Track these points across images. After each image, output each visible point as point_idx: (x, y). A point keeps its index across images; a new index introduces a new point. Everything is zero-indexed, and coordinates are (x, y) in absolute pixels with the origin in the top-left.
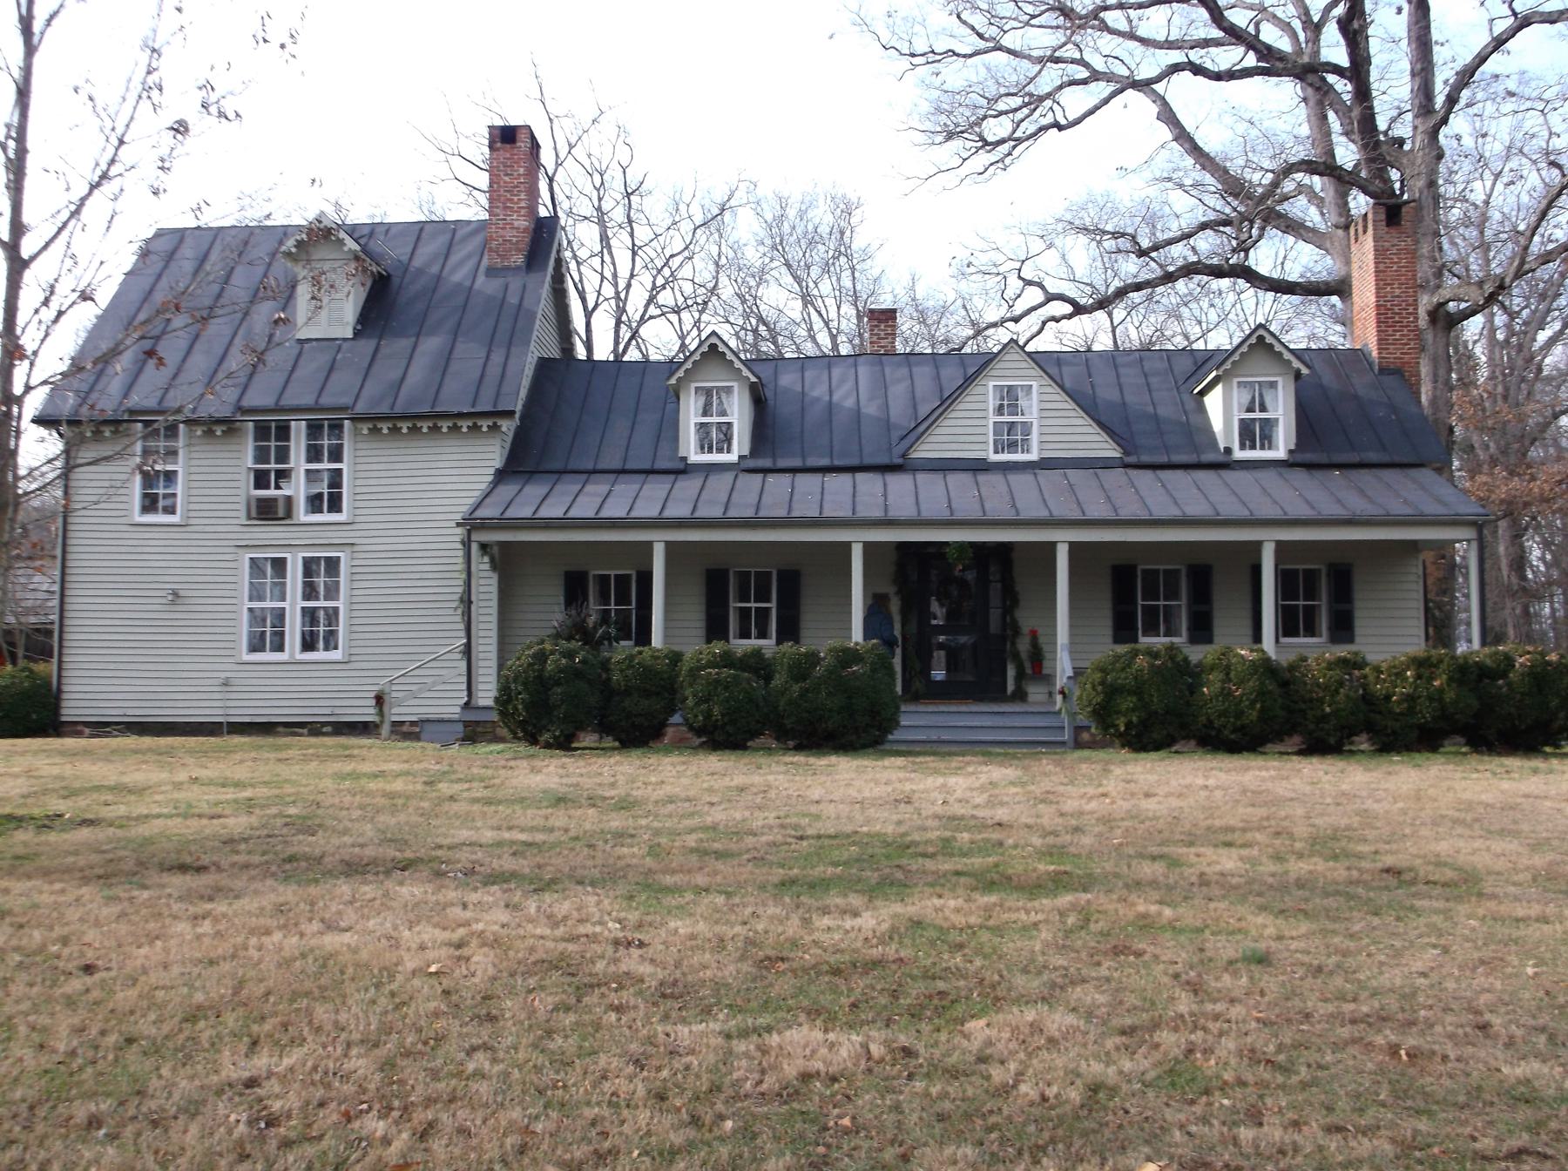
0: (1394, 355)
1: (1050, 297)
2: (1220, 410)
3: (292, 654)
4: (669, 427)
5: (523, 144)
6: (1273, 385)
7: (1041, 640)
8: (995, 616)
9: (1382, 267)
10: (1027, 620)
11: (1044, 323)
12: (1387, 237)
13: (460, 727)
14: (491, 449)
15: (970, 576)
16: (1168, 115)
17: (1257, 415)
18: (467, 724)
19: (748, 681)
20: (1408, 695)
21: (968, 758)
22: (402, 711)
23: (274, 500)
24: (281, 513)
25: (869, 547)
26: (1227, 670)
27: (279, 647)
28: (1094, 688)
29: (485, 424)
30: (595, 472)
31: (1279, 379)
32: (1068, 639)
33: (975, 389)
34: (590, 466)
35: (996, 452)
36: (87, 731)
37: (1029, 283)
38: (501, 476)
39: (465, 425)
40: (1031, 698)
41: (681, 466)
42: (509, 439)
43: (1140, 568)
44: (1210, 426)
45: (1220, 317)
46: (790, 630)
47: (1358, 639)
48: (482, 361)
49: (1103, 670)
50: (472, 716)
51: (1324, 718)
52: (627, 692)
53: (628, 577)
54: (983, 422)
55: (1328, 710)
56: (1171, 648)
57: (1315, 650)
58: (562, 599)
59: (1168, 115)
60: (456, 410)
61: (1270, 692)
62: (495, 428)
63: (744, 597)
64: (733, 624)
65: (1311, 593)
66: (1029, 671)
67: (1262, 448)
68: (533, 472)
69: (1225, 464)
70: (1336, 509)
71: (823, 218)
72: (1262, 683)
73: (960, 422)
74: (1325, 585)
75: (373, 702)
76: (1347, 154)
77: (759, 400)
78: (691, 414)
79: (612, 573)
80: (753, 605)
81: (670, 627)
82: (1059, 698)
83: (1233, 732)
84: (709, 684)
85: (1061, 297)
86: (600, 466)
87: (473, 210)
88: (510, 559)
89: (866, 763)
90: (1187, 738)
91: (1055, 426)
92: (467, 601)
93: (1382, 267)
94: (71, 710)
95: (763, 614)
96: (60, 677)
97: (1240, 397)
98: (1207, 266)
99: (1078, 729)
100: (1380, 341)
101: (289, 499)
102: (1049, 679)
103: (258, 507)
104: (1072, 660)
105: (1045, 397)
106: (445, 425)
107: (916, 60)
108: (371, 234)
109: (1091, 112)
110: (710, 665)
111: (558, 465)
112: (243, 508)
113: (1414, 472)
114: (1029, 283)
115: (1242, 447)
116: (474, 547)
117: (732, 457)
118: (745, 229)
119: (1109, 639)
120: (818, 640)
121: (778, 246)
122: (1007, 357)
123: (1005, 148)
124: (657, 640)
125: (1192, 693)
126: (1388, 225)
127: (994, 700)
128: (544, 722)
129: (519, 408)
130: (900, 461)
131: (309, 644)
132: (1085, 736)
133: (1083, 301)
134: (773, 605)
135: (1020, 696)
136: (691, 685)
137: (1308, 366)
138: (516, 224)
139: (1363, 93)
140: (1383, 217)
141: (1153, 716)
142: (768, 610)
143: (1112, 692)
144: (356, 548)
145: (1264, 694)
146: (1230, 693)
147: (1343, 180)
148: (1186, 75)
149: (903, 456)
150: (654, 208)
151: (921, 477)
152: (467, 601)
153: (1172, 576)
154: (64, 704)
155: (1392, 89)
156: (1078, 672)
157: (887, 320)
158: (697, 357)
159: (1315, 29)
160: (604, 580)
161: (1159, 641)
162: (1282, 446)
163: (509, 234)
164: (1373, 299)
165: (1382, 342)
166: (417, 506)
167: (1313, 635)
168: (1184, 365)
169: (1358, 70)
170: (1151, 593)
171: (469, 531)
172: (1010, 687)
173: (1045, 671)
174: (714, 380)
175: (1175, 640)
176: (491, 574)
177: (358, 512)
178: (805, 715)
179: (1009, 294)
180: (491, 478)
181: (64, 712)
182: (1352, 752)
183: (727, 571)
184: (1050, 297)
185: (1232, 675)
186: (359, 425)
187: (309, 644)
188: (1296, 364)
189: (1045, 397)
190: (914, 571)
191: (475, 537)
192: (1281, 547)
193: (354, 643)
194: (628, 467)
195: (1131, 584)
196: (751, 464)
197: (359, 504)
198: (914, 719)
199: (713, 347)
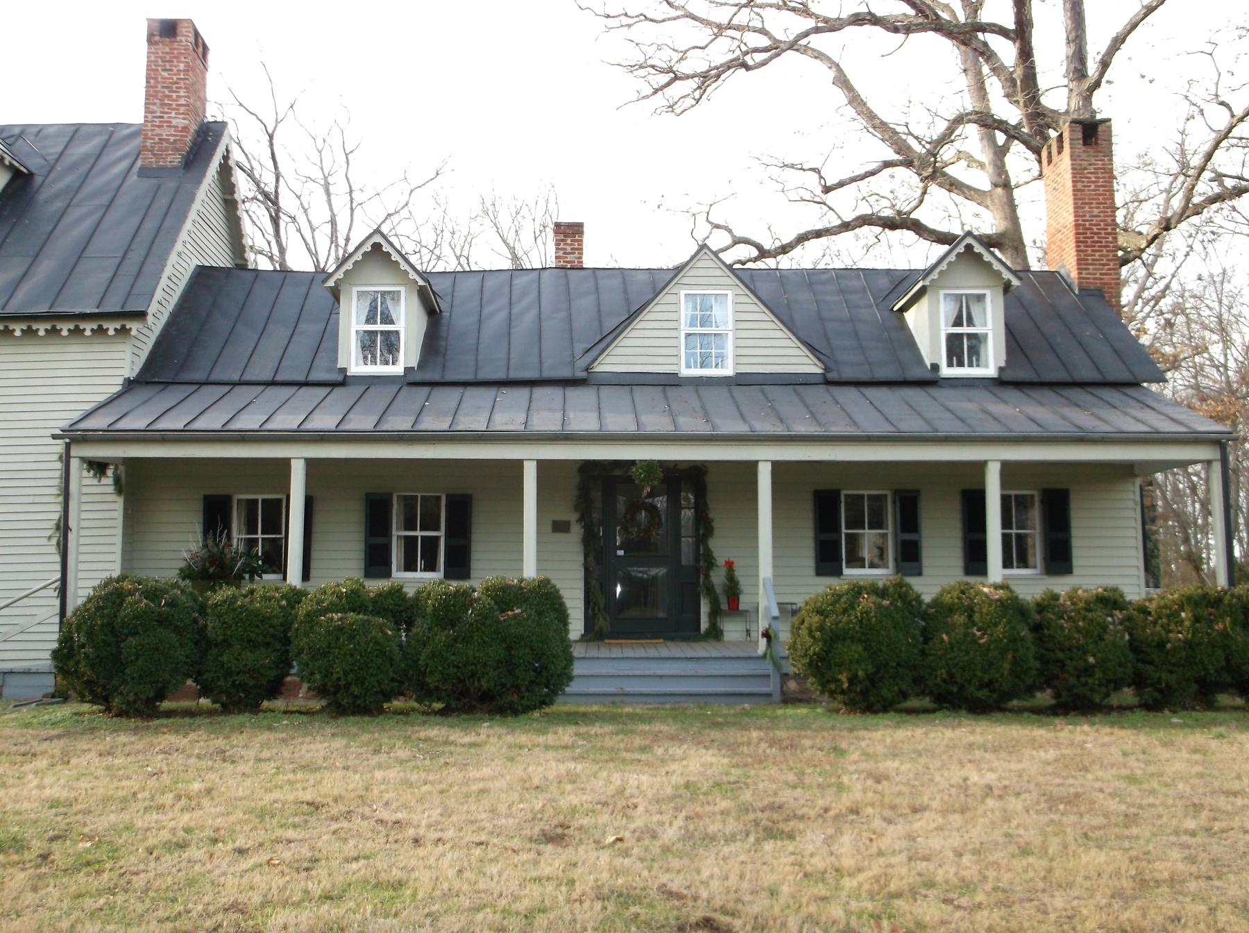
0: (1095, 275)
1: (737, 241)
2: (927, 325)
4: (328, 337)
5: (185, 38)
6: (980, 298)
7: (739, 573)
8: (687, 543)
9: (1079, 185)
10: (722, 548)
12: (1084, 156)
15: (661, 502)
17: (964, 330)
19: (381, 629)
20: (1186, 641)
21: (657, 727)
25: (544, 467)
26: (970, 611)
28: (810, 633)
29: (111, 327)
31: (988, 292)
32: (770, 570)
34: (236, 378)
35: (688, 366)
37: (717, 226)
39: (88, 327)
40: (728, 636)
41: (340, 378)
43: (843, 493)
46: (459, 565)
47: (1076, 571)
48: (117, 261)
49: (820, 612)
51: (1088, 670)
52: (226, 644)
54: (674, 333)
55: (1091, 660)
58: (199, 528)
61: (1022, 639)
62: (123, 331)
63: (410, 525)
64: (397, 555)
66: (724, 606)
67: (971, 365)
68: (168, 384)
69: (930, 382)
70: (1055, 434)
72: (1013, 628)
78: (353, 321)
79: (260, 497)
80: (419, 533)
82: (763, 642)
83: (980, 687)
84: (329, 633)
85: (747, 242)
87: (135, 115)
89: (523, 738)
93: (1079, 185)
95: (430, 545)
97: (946, 310)
98: (880, 218)
100: (1080, 262)
102: (749, 615)
106: (65, 328)
108: (20, 136)
110: (333, 608)
111: (200, 376)
114: (717, 226)
115: (950, 364)
116: (75, 463)
117: (397, 369)
119: (812, 571)
120: (485, 573)
125: (926, 641)
126: (1085, 144)
127: (685, 639)
128: (115, 682)
130: (581, 374)
133: (767, 247)
134: (441, 533)
135: (715, 633)
136: (306, 635)
138: (174, 122)
140: (1080, 135)
141: (889, 667)
142: (437, 538)
143: (832, 639)
145: (1015, 641)
146: (974, 641)
151: (605, 391)
153: (878, 501)
156: (788, 611)
157: (574, 234)
158: (358, 257)
162: (991, 363)
163: (165, 133)
164: (1071, 218)
165: (1081, 263)
167: (1026, 566)
168: (884, 283)
170: (856, 522)
171: (68, 447)
172: (704, 625)
174: (379, 283)
176: (114, 497)
178: (452, 670)
183: (391, 495)
184: (737, 241)
185: (977, 617)
190: (600, 498)
191: (76, 451)
194: (279, 378)
195: (831, 510)
196: (418, 377)
199: (377, 247)
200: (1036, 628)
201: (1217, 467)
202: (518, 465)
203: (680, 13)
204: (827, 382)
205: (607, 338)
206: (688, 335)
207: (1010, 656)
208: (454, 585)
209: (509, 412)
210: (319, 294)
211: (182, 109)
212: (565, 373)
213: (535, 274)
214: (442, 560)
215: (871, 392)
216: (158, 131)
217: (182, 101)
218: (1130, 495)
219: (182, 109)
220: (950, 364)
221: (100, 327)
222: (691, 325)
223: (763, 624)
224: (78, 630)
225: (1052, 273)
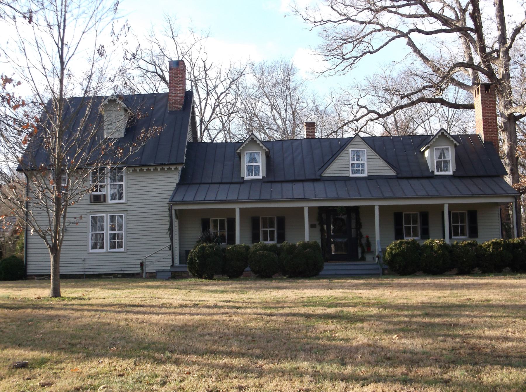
1: (369, 112)
3: (107, 250)
6: (447, 149)
7: (370, 239)
8: (353, 231)
9: (484, 106)
10: (365, 232)
11: (367, 121)
13: (170, 274)
14: (175, 176)
16: (410, 43)
17: (442, 159)
18: (172, 272)
22: (150, 269)
23: (100, 196)
24: (102, 200)
25: (310, 209)
27: (102, 247)
30: (212, 183)
31: (450, 147)
33: (345, 152)
34: (210, 182)
35: (352, 173)
36: (36, 278)
38: (179, 185)
40: (367, 259)
41: (242, 181)
42: (180, 172)
43: (403, 213)
44: (375, 237)
45: (431, 121)
46: (281, 238)
50: (173, 270)
53: (224, 220)
54: (347, 163)
55: (465, 260)
56: (414, 240)
57: (462, 240)
59: (410, 43)
60: (163, 163)
62: (176, 169)
65: (462, 221)
66: (366, 250)
67: (445, 171)
69: (431, 176)
71: (279, 76)
73: (339, 163)
74: (468, 220)
75: (140, 266)
76: (477, 59)
77: (268, 157)
78: (245, 163)
80: (268, 229)
81: (241, 237)
82: (377, 259)
86: (213, 181)
88: (181, 216)
90: (419, 271)
91: (372, 165)
92: (171, 230)
94: (31, 270)
96: (26, 259)
97: (436, 154)
98: (427, 99)
99: (383, 270)
101: (104, 195)
102: (373, 253)
103: (94, 198)
104: (381, 246)
105: (369, 154)
107: (316, 24)
109: (382, 47)
112: (88, 198)
113: (495, 179)
115: (438, 171)
117: (260, 177)
118: (249, 81)
121: (262, 87)
122: (356, 140)
123: (351, 61)
124: (237, 242)
129: (184, 162)
130: (318, 177)
131: (113, 246)
132: (386, 272)
134: (275, 229)
135: (363, 259)
137: (458, 143)
138: (179, 95)
139: (481, 38)
144: (128, 212)
147: (476, 68)
148: (416, 33)
149: (320, 176)
150: (212, 74)
151: (326, 182)
152: (171, 230)
154: (28, 268)
155: (491, 35)
159: (464, 11)
160: (215, 222)
161: (410, 239)
163: (177, 99)
164: (482, 117)
166: (148, 196)
167: (464, 235)
169: (478, 29)
173: (371, 250)
175: (415, 238)
177: (129, 199)
179: (355, 111)
180: (175, 186)
181: (28, 271)
182: (473, 274)
183: (259, 217)
184: (369, 112)
186: (129, 169)
187: (113, 246)
188: (455, 142)
189: (369, 154)
190: (323, 216)
192: (450, 205)
193: (128, 245)
194: (223, 181)
195: (398, 220)
196: (266, 180)
197: (129, 196)
198: (328, 267)
200: (451, 252)
201: (514, 204)
202: (302, 209)
203: (344, 17)
204: (398, 178)
205: (326, 164)
206: (352, 164)
207: (442, 259)
208: (279, 245)
209: (298, 190)
210: (231, 152)
211: (181, 91)
212: (313, 177)
213: (299, 141)
214: (276, 237)
215: (412, 182)
216: (174, 98)
217: (181, 88)
218: (497, 211)
219: (181, 91)
220: (438, 171)
221: (169, 168)
222: (353, 160)
223: (377, 254)
224: (195, 256)
225: (476, 135)
